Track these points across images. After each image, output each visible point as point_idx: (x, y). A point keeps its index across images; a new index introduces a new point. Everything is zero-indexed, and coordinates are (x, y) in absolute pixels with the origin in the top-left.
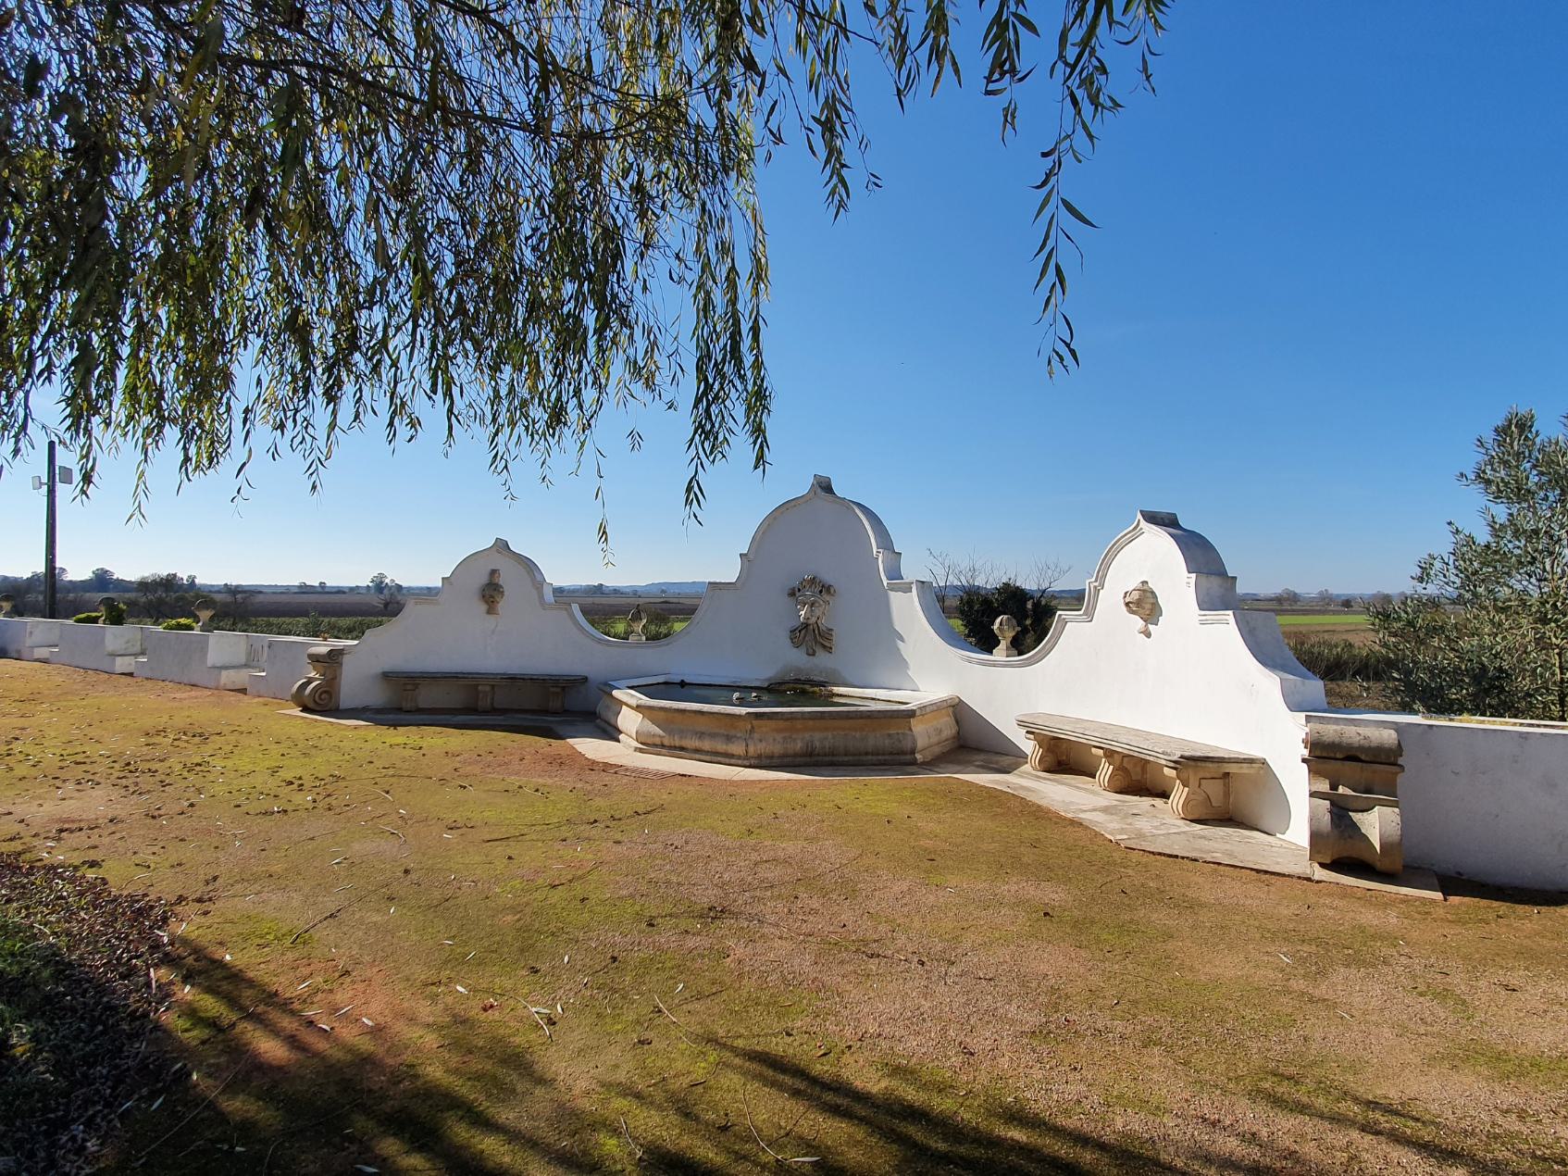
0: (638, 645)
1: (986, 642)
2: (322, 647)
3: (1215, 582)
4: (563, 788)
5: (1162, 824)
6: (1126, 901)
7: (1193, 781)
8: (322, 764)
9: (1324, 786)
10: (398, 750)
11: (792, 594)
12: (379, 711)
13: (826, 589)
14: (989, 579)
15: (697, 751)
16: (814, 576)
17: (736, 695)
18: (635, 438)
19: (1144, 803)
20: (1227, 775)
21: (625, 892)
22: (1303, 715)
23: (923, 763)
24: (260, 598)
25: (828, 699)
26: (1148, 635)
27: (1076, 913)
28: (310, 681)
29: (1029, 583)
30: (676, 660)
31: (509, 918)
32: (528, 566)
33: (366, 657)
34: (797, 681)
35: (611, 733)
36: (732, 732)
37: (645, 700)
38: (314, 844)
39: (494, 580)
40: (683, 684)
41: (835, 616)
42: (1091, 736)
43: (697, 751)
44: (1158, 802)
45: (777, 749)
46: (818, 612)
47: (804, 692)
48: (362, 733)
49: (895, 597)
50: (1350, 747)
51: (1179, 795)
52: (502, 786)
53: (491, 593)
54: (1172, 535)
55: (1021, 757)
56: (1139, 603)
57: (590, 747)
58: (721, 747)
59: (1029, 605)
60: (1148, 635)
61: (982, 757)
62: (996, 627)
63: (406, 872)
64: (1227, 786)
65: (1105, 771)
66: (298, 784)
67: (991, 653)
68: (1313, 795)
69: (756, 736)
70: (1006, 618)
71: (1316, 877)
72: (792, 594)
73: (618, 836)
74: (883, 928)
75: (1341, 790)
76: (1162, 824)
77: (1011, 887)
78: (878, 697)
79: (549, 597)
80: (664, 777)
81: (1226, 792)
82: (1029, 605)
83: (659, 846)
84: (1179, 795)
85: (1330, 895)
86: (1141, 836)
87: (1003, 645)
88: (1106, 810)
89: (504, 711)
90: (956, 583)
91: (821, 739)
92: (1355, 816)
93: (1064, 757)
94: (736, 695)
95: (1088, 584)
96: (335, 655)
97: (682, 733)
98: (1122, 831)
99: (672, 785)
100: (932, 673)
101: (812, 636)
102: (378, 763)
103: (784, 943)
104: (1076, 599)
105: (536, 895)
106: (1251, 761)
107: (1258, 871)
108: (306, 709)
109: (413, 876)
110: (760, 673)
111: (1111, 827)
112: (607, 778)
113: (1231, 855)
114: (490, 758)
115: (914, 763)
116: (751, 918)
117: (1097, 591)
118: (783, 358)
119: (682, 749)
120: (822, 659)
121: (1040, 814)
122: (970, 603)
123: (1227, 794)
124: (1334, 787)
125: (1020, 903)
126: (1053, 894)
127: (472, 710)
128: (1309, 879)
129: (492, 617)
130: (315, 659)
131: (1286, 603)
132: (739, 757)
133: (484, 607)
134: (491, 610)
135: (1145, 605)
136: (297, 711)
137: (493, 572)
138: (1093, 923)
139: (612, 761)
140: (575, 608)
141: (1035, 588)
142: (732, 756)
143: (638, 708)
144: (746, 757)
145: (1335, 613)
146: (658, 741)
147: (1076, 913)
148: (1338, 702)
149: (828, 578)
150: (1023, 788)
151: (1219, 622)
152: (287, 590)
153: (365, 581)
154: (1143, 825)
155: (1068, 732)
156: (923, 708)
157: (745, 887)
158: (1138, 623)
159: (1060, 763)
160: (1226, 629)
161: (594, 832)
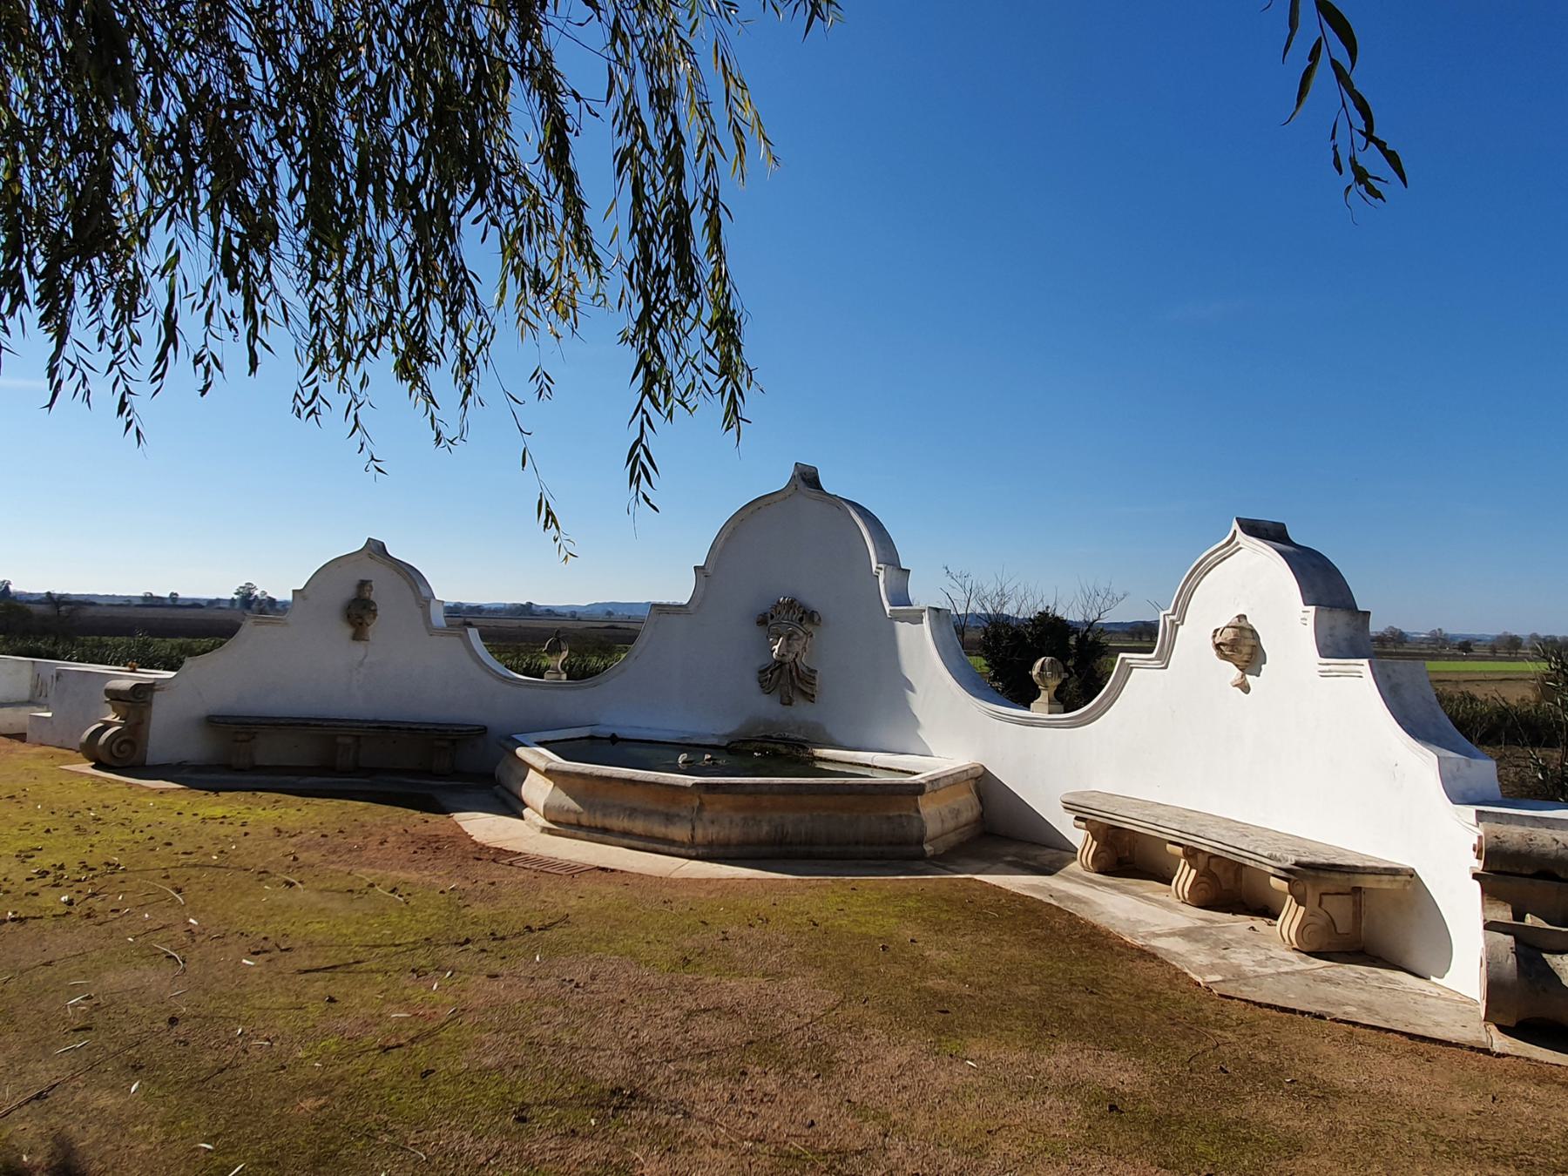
0: (558, 686)
1: (1019, 692)
2: (124, 679)
3: (1341, 618)
4: (431, 886)
5: (1264, 957)
6: (1228, 1084)
7: (1312, 898)
8: (108, 845)
9: (1504, 914)
10: (212, 827)
11: (763, 621)
12: (198, 769)
13: (808, 616)
14: (1021, 606)
15: (626, 834)
16: (793, 595)
17: (682, 758)
18: (542, 381)
19: (1240, 924)
20: (1357, 890)
21: (489, 1061)
22: (1472, 809)
23: (934, 857)
24: (91, 611)
25: (808, 766)
26: (1246, 688)
27: (1156, 1105)
28: (107, 725)
29: (1072, 613)
30: (614, 704)
31: (309, 1104)
32: (411, 576)
33: (187, 691)
34: (767, 738)
35: (512, 806)
36: (674, 810)
37: (558, 762)
38: (50, 971)
39: (366, 591)
40: (614, 739)
41: (824, 654)
42: (1169, 828)
43: (626, 834)
44: (1260, 923)
45: (735, 833)
46: (797, 647)
47: (776, 754)
48: (168, 799)
49: (903, 629)
50: (1543, 857)
51: (1291, 916)
52: (344, 884)
53: (359, 612)
54: (1281, 553)
55: (1066, 851)
56: (1234, 645)
57: (481, 826)
58: (658, 829)
59: (1072, 641)
60: (1246, 688)
61: (1014, 849)
62: (1034, 673)
63: (173, 1021)
64: (1358, 905)
65: (1185, 876)
66: (55, 876)
67: (1027, 707)
68: (1489, 926)
69: (706, 815)
70: (1047, 661)
71: (1496, 1048)
72: (763, 621)
73: (496, 966)
74: (870, 1129)
75: (1530, 920)
76: (1264, 957)
77: (1064, 1059)
78: (881, 763)
79: (438, 618)
80: (575, 872)
81: (1359, 914)
82: (1072, 641)
83: (552, 981)
84: (1291, 916)
85: (1522, 1078)
86: (1239, 976)
87: (1044, 697)
88: (1186, 934)
89: (371, 772)
90: (979, 610)
91: (794, 821)
92: (1554, 960)
93: (1127, 854)
94: (682, 758)
95: (1163, 617)
96: (142, 692)
97: (606, 809)
98: (1213, 968)
99: (585, 884)
100: (948, 734)
101: (788, 680)
102: (179, 847)
103: (718, 1154)
104: (1143, 636)
105: (357, 1063)
106: (1394, 872)
107: (1411, 1036)
108: (99, 765)
109: (181, 1029)
110: (717, 726)
111: (1196, 961)
112: (497, 872)
113: (1369, 1010)
114: (339, 839)
115: (922, 856)
116: (674, 1107)
117: (1175, 627)
118: (757, 255)
119: (605, 831)
120: (802, 711)
121: (1096, 942)
122: (996, 637)
123: (1357, 915)
124: (1518, 916)
125: (1071, 1088)
126: (1121, 1073)
127: (327, 769)
128: (1487, 1052)
129: (360, 646)
130: (115, 696)
131: (1440, 646)
132: (682, 844)
133: (349, 631)
134: (359, 635)
135: (1242, 648)
136: (86, 767)
137: (363, 584)
138: (1181, 1123)
139: (509, 846)
140: (473, 633)
141: (1079, 618)
142: (672, 842)
143: (548, 773)
144: (692, 843)
145: (1454, 657)
146: (572, 819)
147: (1156, 1105)
148: (1520, 792)
149: (812, 601)
150: (1077, 899)
151: (1348, 674)
152: (127, 603)
153: (228, 593)
154: (1243, 959)
155: (1133, 820)
156: (934, 781)
157: (670, 1052)
158: (1232, 671)
159: (1120, 862)
160: (1358, 684)
161: (463, 960)
